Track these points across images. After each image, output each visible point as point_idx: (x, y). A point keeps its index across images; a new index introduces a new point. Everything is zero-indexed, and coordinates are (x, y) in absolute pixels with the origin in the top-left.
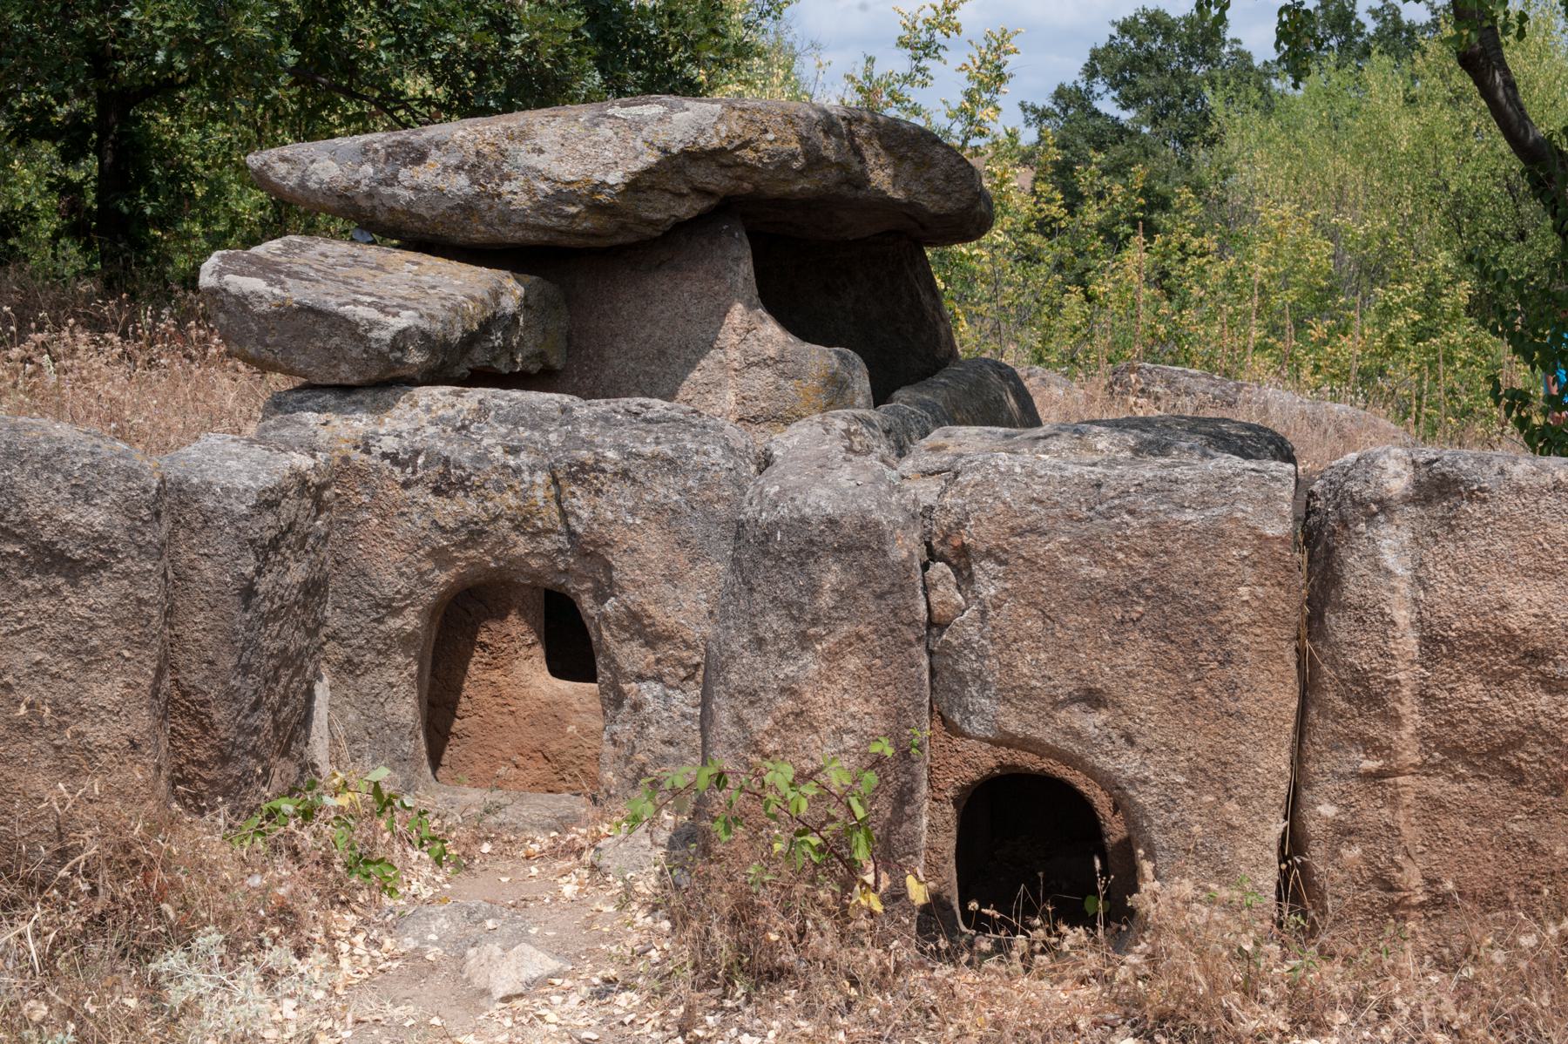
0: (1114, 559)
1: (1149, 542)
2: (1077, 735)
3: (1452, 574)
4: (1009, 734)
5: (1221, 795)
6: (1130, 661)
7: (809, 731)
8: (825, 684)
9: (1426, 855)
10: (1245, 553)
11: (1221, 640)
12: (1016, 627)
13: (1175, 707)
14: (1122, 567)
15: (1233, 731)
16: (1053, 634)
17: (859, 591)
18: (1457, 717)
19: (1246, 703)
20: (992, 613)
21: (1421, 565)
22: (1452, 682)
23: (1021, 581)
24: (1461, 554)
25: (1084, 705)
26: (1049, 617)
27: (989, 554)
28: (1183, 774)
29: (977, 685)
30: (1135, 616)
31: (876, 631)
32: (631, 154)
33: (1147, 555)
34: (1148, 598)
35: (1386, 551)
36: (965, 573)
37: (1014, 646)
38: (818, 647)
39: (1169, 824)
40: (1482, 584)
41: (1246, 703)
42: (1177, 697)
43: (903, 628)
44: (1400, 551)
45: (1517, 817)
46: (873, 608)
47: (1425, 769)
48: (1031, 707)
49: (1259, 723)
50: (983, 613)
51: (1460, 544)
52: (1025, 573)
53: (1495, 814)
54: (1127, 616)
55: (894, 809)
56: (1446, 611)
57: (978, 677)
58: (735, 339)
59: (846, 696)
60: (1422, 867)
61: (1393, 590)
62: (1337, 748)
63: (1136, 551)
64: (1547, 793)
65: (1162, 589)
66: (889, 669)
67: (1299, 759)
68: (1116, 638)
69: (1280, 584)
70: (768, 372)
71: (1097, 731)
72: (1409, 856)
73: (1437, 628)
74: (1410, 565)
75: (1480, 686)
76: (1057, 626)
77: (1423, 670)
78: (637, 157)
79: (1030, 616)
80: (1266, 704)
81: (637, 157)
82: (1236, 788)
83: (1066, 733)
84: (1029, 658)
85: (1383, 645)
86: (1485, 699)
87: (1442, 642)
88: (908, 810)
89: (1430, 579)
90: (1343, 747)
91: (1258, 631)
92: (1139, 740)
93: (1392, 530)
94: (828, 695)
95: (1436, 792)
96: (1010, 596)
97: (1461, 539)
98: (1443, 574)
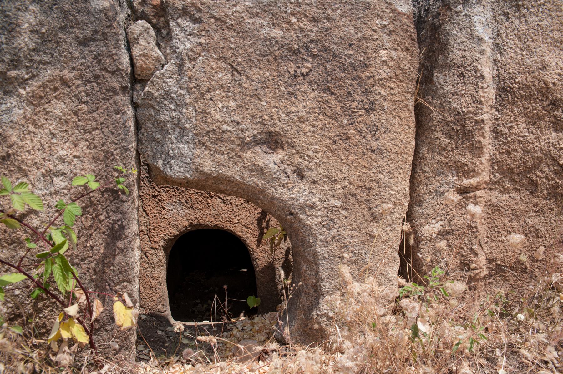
0: (289, 22)
1: (315, 9)
2: (260, 171)
3: (517, 42)
4: (205, 174)
5: (366, 213)
6: (301, 108)
7: (18, 175)
8: (31, 128)
9: (488, 244)
10: (385, 23)
11: (367, 92)
12: (209, 78)
13: (334, 146)
14: (295, 29)
15: (374, 164)
16: (240, 85)
17: (60, 35)
18: (512, 147)
19: (384, 142)
20: (188, 65)
21: (498, 35)
22: (511, 122)
23: (213, 38)
24: (523, 27)
25: (265, 147)
26: (237, 70)
27: (185, 12)
28: (339, 199)
29: (176, 132)
30: (305, 71)
31: (81, 77)
33: (314, 20)
34: (314, 56)
35: (477, 24)
36: (164, 32)
37: (208, 96)
38: (22, 91)
39: (329, 239)
40: (534, 50)
41: (384, 142)
42: (336, 138)
43: (107, 75)
44: (487, 25)
45: (531, 214)
46: (77, 54)
47: (491, 185)
48: (223, 149)
49: (392, 157)
50: (180, 66)
51: (523, 19)
52: (216, 31)
53: (522, 214)
54: (298, 71)
55: (108, 244)
56: (513, 68)
57: (177, 125)
59: (54, 140)
60: (487, 252)
61: (482, 52)
62: (439, 174)
63: (306, 16)
64: (546, 198)
65: (325, 49)
66: (95, 114)
67: (413, 186)
68: (290, 89)
69: (407, 49)
71: (276, 167)
72: (481, 245)
73: (508, 81)
74: (492, 36)
75: (524, 125)
76: (244, 78)
77: (496, 113)
79: (221, 69)
80: (397, 142)
82: (376, 207)
83: (251, 170)
84: (220, 105)
85: (475, 94)
86: (527, 134)
87: (510, 92)
88: (120, 244)
89: (504, 45)
90: (443, 173)
91: (393, 85)
92: (308, 174)
93: (481, 9)
94: (35, 140)
95: (494, 200)
96: (204, 50)
97: (524, 16)
98: (511, 41)
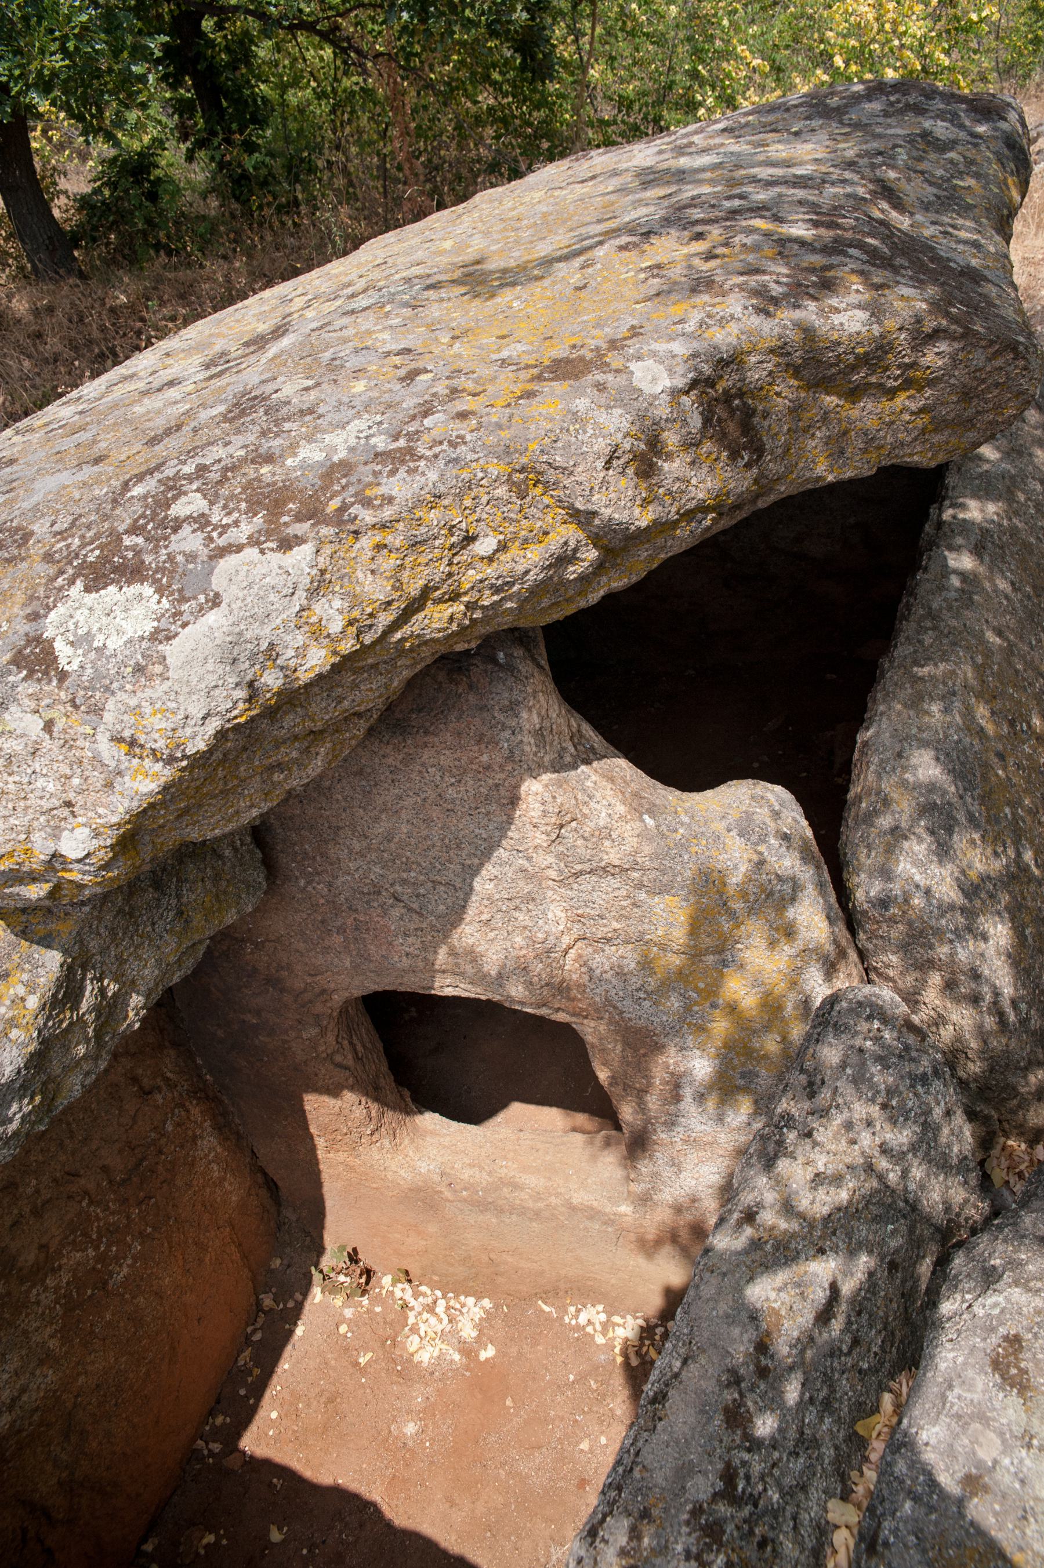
32: (97, 778)
58: (541, 839)
70: (615, 883)
78: (109, 785)
81: (109, 785)
